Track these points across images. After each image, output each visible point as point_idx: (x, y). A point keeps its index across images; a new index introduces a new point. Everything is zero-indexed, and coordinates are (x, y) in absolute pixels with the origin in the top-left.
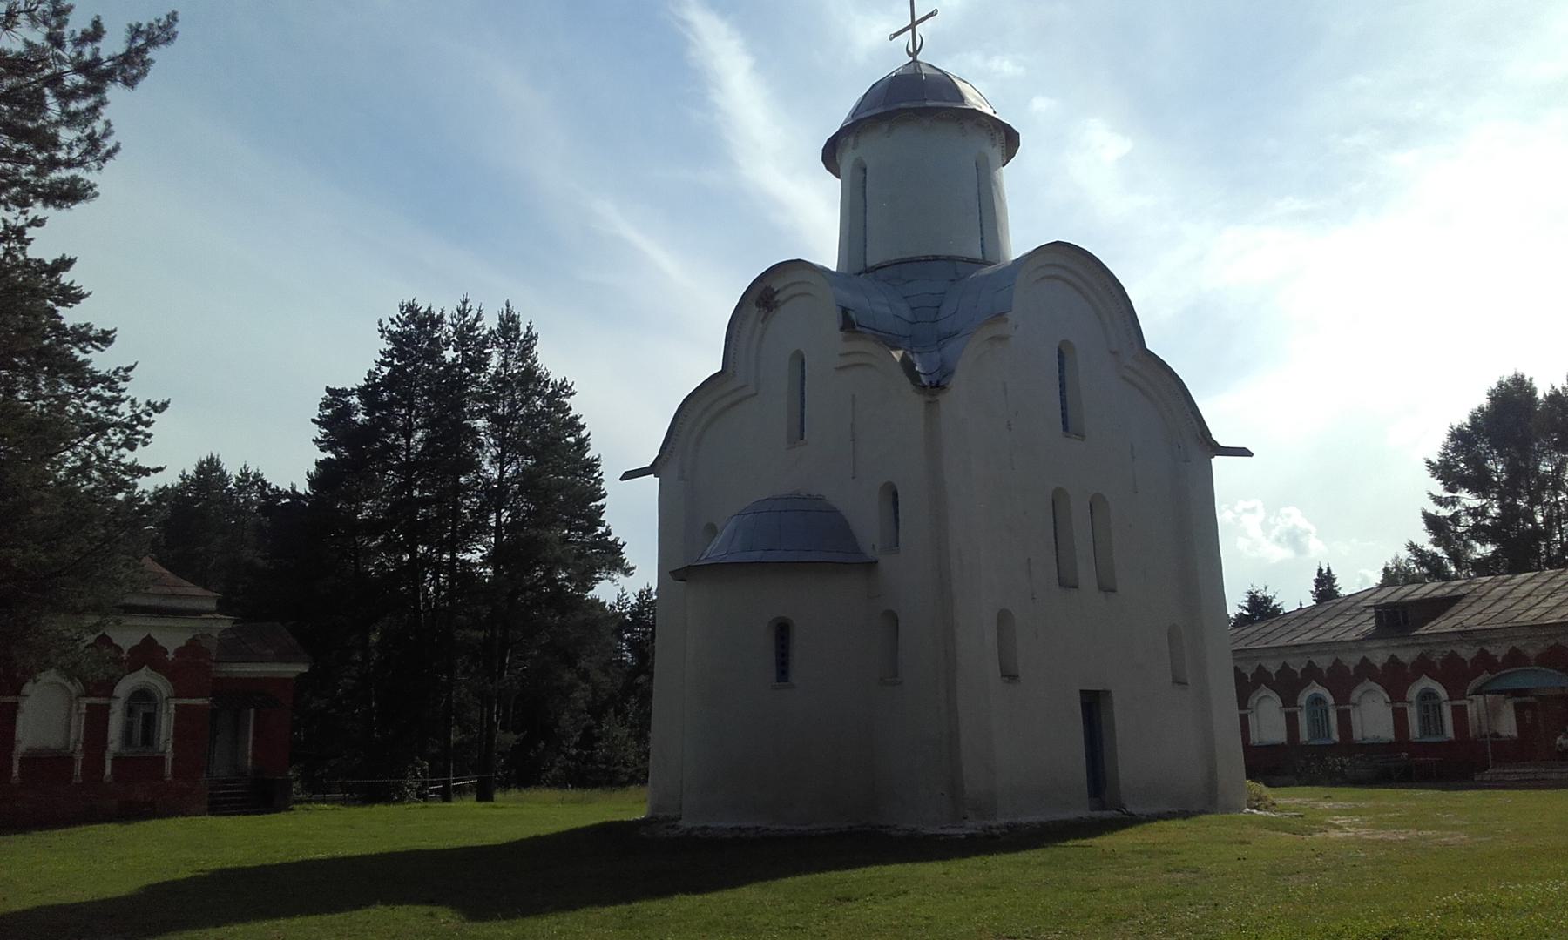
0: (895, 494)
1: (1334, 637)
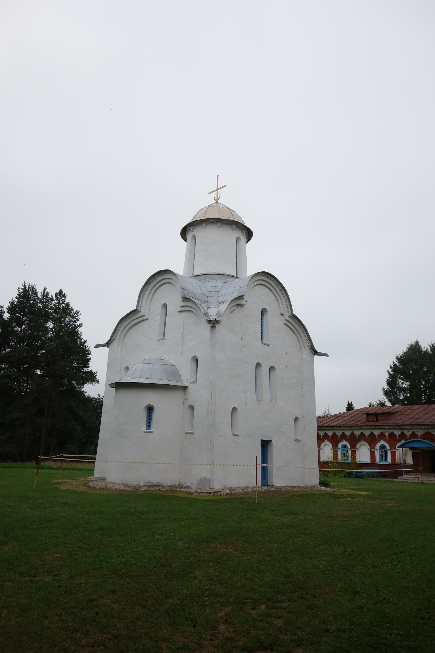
0: (197, 361)
1: (352, 424)
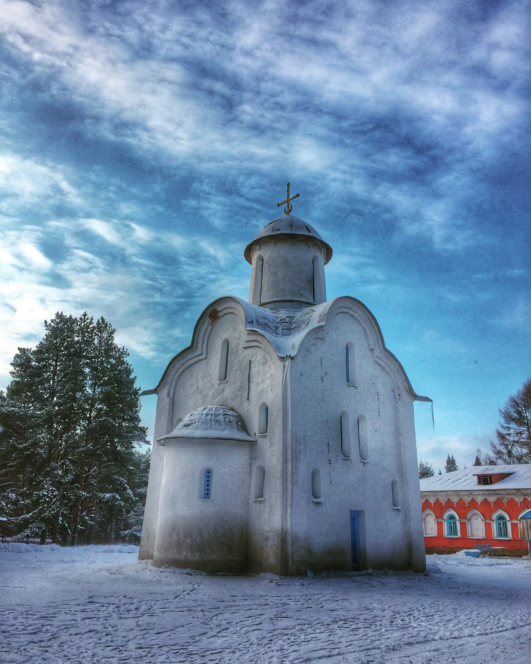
0: (267, 409)
